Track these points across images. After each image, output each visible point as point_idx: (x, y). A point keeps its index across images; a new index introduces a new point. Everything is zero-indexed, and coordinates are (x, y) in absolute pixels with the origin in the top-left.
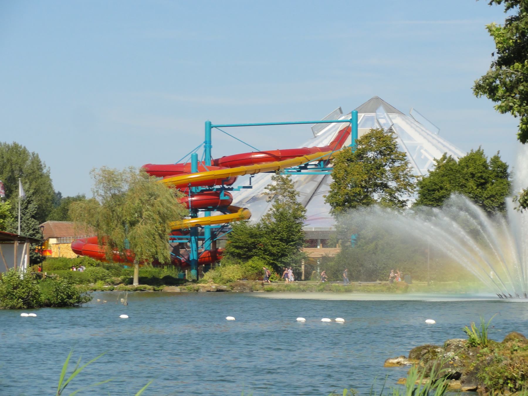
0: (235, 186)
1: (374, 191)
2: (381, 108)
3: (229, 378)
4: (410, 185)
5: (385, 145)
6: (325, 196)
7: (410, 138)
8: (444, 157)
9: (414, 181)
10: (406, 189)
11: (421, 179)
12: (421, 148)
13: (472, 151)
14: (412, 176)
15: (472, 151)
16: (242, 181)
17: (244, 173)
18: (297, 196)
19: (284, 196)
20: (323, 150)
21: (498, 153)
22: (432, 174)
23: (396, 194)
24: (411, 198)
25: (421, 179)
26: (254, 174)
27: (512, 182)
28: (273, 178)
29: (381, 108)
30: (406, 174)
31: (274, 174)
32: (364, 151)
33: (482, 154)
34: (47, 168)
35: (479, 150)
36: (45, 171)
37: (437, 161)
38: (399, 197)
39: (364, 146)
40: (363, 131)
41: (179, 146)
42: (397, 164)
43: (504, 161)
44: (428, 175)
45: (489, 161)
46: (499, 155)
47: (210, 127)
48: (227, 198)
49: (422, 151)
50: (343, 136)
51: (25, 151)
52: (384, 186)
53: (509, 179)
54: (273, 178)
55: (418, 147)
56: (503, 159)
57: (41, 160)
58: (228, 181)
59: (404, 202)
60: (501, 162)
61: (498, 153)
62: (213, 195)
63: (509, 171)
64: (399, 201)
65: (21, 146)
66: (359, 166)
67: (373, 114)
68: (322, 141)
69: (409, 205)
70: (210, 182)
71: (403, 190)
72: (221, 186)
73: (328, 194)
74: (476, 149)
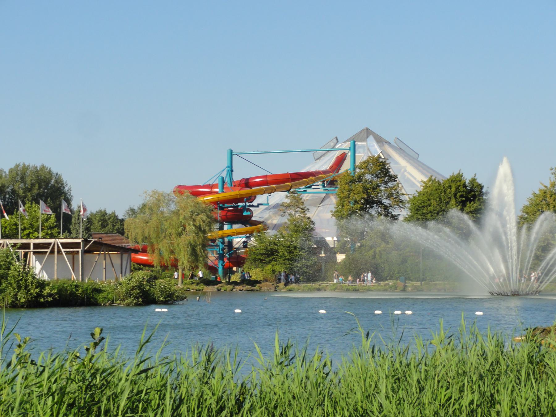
0: (255, 203)
1: (371, 207)
2: (371, 137)
3: (304, 363)
4: (401, 202)
5: (382, 169)
6: (332, 212)
7: (397, 163)
8: (430, 180)
9: (406, 198)
10: (398, 205)
11: (411, 197)
12: (405, 171)
13: (453, 174)
14: (403, 194)
15: (453, 174)
16: (260, 199)
17: (263, 192)
18: (306, 212)
19: (296, 211)
20: (324, 172)
21: (475, 175)
22: (420, 193)
23: (390, 210)
24: (403, 213)
25: (411, 197)
26: (270, 193)
27: (486, 199)
28: (287, 197)
29: (371, 137)
30: (398, 193)
31: (287, 193)
32: (363, 174)
33: (462, 176)
34: (68, 186)
35: (459, 173)
36: (66, 189)
37: (425, 183)
38: (392, 211)
39: (363, 170)
40: (361, 157)
41: (206, 171)
42: (390, 185)
43: (480, 183)
44: (417, 194)
45: (467, 182)
46: (476, 178)
47: (232, 153)
48: (249, 213)
49: (405, 173)
50: (341, 160)
51: (50, 172)
52: (379, 203)
53: (484, 197)
54: (287, 197)
55: (403, 170)
56: (479, 181)
57: (64, 179)
58: (251, 198)
59: (396, 216)
60: (477, 183)
61: (475, 175)
62: (235, 211)
63: (484, 190)
64: (392, 215)
65: (29, 166)
66: (358, 186)
67: (364, 143)
68: (322, 166)
69: (401, 218)
70: (237, 200)
71: (396, 206)
72: (244, 204)
73: (334, 210)
74: (456, 173)
